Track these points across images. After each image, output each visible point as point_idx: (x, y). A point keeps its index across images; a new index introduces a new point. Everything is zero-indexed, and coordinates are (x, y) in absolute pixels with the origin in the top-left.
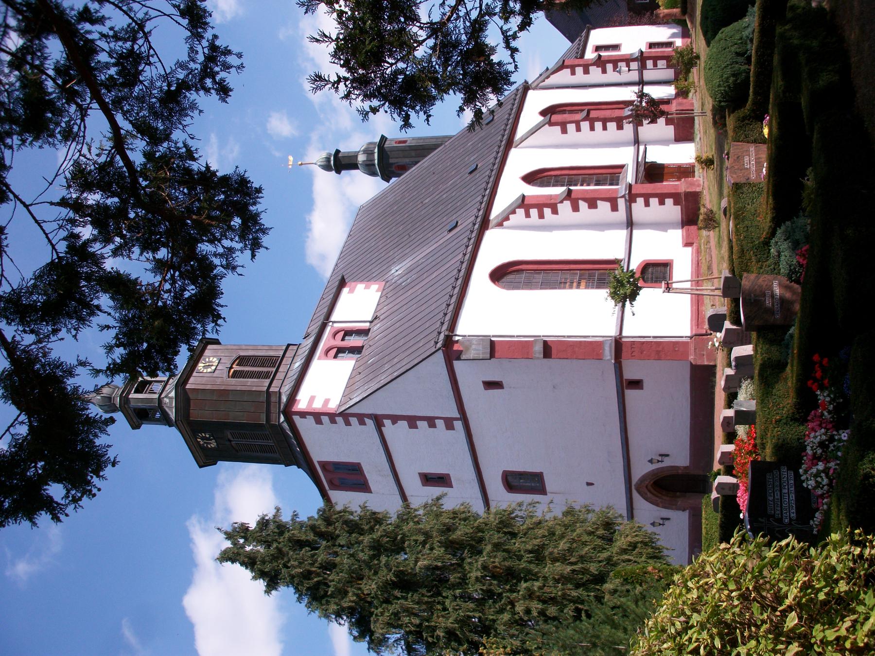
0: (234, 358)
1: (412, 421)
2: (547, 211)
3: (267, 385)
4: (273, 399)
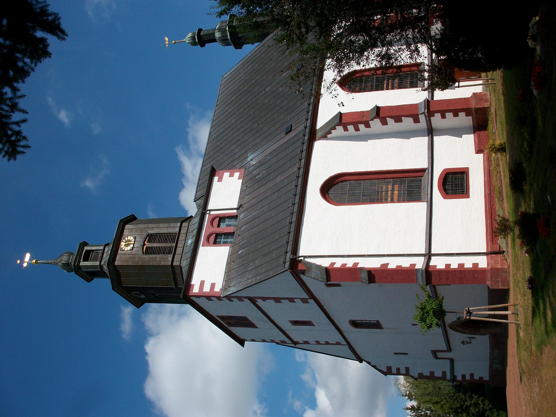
0: (144, 236)
1: (278, 300)
2: (362, 127)
3: (170, 259)
4: (177, 271)
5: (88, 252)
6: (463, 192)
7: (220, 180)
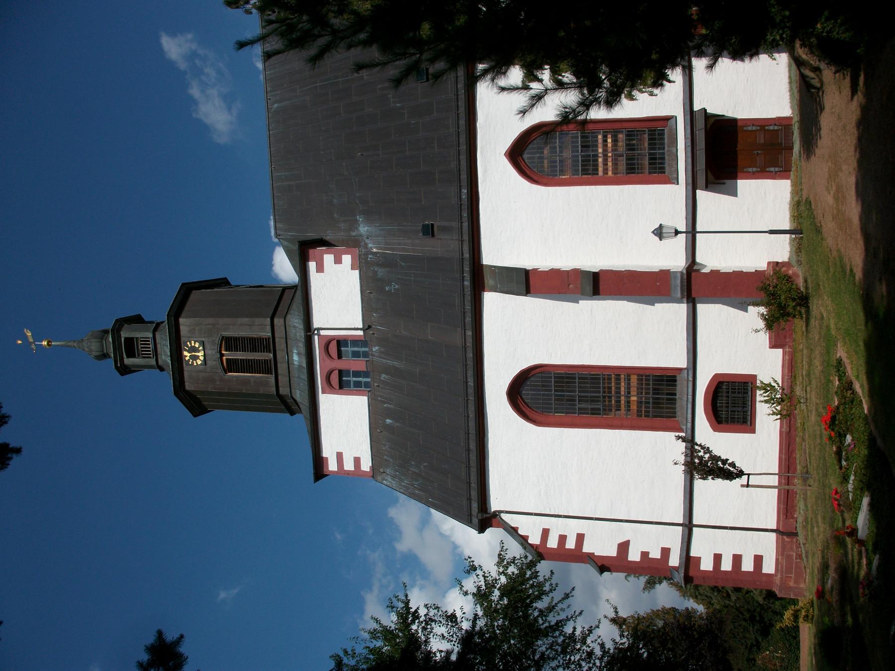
0: (217, 341)
3: (273, 380)
5: (130, 341)
6: (744, 422)
7: (320, 269)
